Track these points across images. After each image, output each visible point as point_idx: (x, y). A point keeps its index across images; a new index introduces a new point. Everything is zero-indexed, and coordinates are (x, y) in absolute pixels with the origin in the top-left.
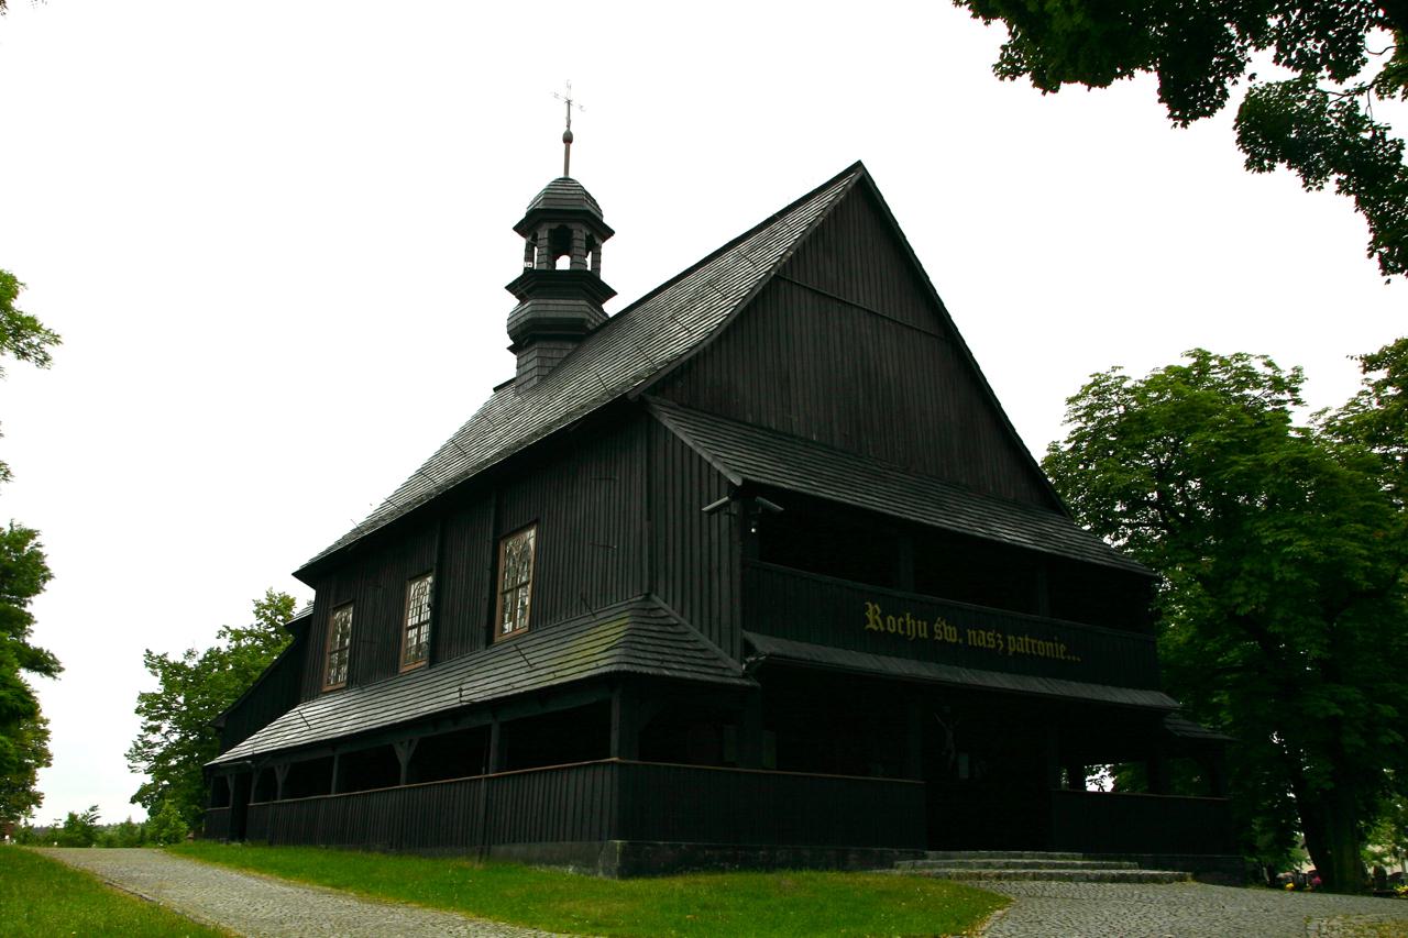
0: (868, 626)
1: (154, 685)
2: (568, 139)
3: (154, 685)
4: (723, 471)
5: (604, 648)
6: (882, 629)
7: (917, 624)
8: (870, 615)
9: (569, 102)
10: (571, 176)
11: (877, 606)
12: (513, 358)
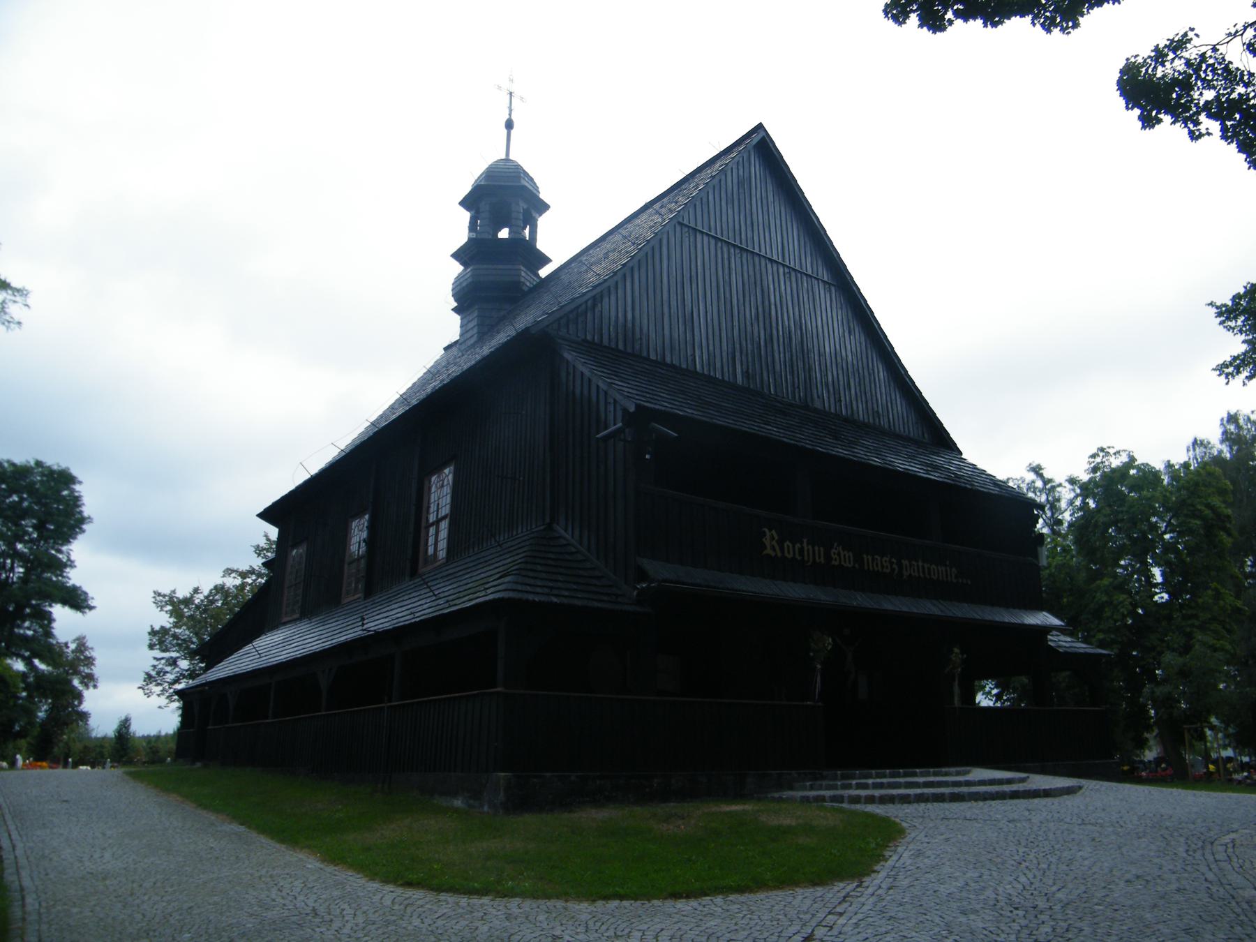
0: (765, 552)
1: (164, 619)
2: (509, 125)
3: (164, 619)
4: (618, 397)
5: (498, 576)
6: (779, 554)
7: (814, 551)
8: (767, 541)
9: (511, 94)
10: (511, 157)
11: (774, 532)
12: (457, 319)
